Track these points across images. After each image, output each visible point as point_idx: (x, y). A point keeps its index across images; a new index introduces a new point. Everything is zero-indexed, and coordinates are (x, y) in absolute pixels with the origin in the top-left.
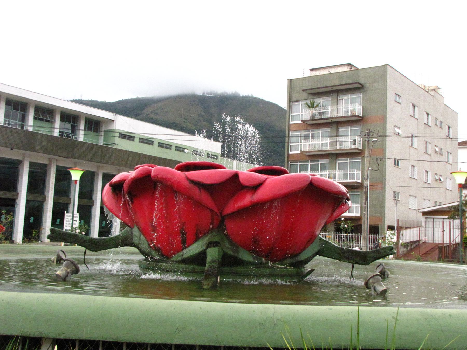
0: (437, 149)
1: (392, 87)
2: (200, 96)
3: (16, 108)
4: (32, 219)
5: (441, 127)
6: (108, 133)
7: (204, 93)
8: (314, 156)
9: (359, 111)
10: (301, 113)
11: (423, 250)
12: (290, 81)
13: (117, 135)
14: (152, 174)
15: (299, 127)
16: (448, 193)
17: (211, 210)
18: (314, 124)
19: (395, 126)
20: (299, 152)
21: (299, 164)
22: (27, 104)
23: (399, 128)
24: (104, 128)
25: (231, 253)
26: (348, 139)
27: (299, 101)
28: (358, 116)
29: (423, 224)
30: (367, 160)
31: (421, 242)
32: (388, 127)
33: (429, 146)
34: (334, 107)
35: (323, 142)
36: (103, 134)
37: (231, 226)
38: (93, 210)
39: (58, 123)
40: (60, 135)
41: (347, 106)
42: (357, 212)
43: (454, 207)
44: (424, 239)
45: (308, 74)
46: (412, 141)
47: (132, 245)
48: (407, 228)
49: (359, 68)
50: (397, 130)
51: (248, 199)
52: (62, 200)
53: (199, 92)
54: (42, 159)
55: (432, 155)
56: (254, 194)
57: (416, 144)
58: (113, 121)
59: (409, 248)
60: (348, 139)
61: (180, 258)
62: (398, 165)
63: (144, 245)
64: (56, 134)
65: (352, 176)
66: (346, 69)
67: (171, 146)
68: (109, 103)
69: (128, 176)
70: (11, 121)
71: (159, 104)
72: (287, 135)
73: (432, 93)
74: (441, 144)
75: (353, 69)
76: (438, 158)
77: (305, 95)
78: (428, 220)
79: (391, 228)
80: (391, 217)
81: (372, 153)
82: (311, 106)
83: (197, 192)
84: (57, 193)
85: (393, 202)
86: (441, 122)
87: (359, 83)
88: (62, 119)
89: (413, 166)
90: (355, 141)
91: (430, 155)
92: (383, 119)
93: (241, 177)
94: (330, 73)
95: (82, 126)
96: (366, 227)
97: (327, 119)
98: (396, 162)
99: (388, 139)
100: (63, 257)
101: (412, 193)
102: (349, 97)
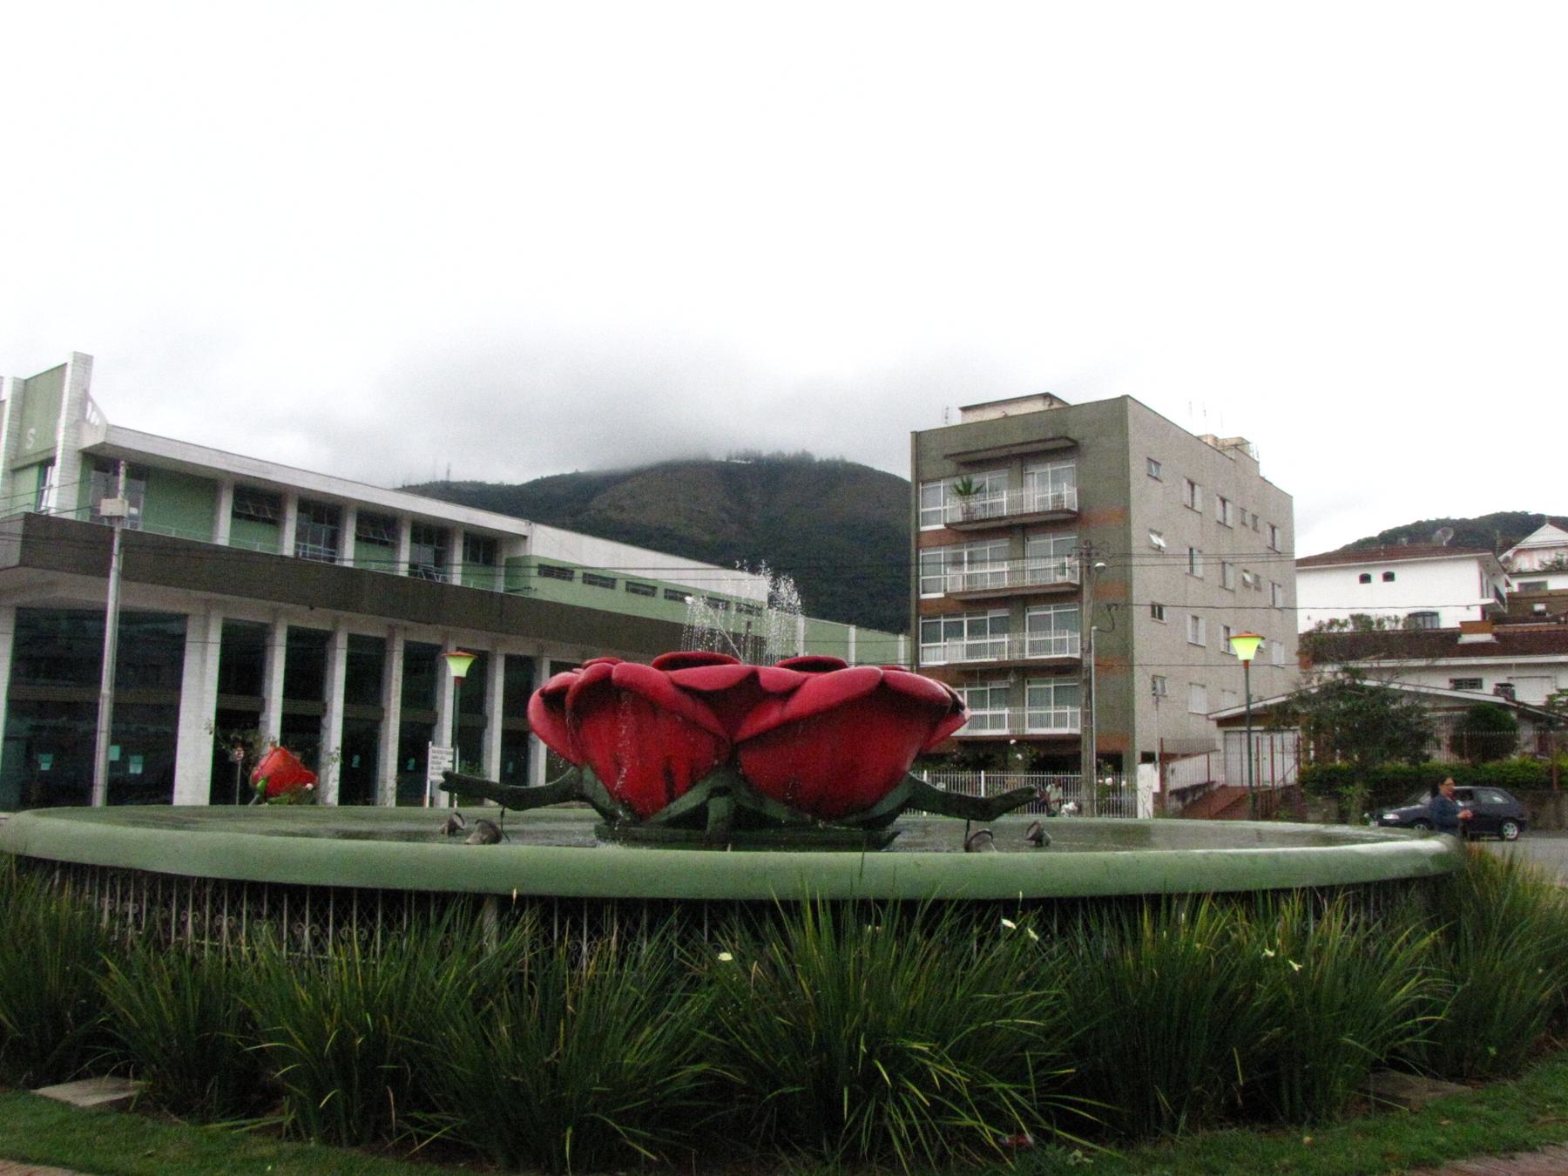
0: (1248, 578)
1: (1139, 447)
2: (721, 463)
3: (318, 519)
4: (356, 759)
5: (1255, 529)
6: (516, 566)
7: (729, 458)
8: (975, 604)
9: (1069, 496)
10: (941, 508)
11: (1220, 803)
12: (917, 437)
13: (534, 572)
14: (614, 676)
15: (939, 539)
16: (1277, 673)
17: (715, 735)
18: (973, 532)
19: (1152, 531)
20: (941, 595)
21: (943, 620)
22: (340, 508)
23: (1159, 535)
24: (505, 555)
25: (749, 805)
26: (1049, 564)
27: (939, 480)
28: (1069, 511)
29: (1220, 745)
30: (1087, 610)
31: (1216, 786)
32: (1135, 533)
33: (1230, 572)
34: (1016, 494)
35: (994, 571)
36: (503, 571)
37: (749, 761)
38: (486, 738)
39: (405, 553)
40: (411, 573)
41: (1043, 490)
42: (1073, 725)
43: (1277, 706)
44: (1219, 777)
45: (957, 419)
46: (1191, 564)
47: (583, 798)
48: (1185, 756)
49: (1072, 403)
50: (1156, 540)
51: (775, 715)
52: (419, 715)
53: (719, 455)
54: (372, 627)
55: (1238, 591)
56: (784, 705)
57: (1199, 571)
58: (525, 537)
59: (1189, 800)
60: (1049, 564)
61: (664, 818)
62: (1161, 617)
63: (605, 799)
64: (403, 570)
65: (1061, 645)
66: (1039, 406)
67: (654, 588)
68: (511, 487)
69: (573, 679)
70: (309, 545)
71: (629, 485)
72: (913, 561)
73: (1231, 454)
74: (1259, 568)
75: (1056, 405)
76: (1250, 598)
77: (950, 466)
78: (1230, 736)
79: (1148, 758)
80: (1149, 729)
81: (1096, 594)
82: (965, 491)
83: (688, 703)
84: (408, 700)
85: (1151, 700)
86: (1255, 517)
87: (1067, 438)
88: (415, 539)
89: (1196, 618)
90: (1063, 567)
91: (1233, 591)
92: (1125, 514)
93: (762, 677)
94: (1006, 417)
95: (458, 555)
96: (1089, 756)
97: (1001, 518)
98: (1157, 611)
99: (1135, 561)
100: (459, 823)
101: (1195, 678)
102: (1049, 469)
